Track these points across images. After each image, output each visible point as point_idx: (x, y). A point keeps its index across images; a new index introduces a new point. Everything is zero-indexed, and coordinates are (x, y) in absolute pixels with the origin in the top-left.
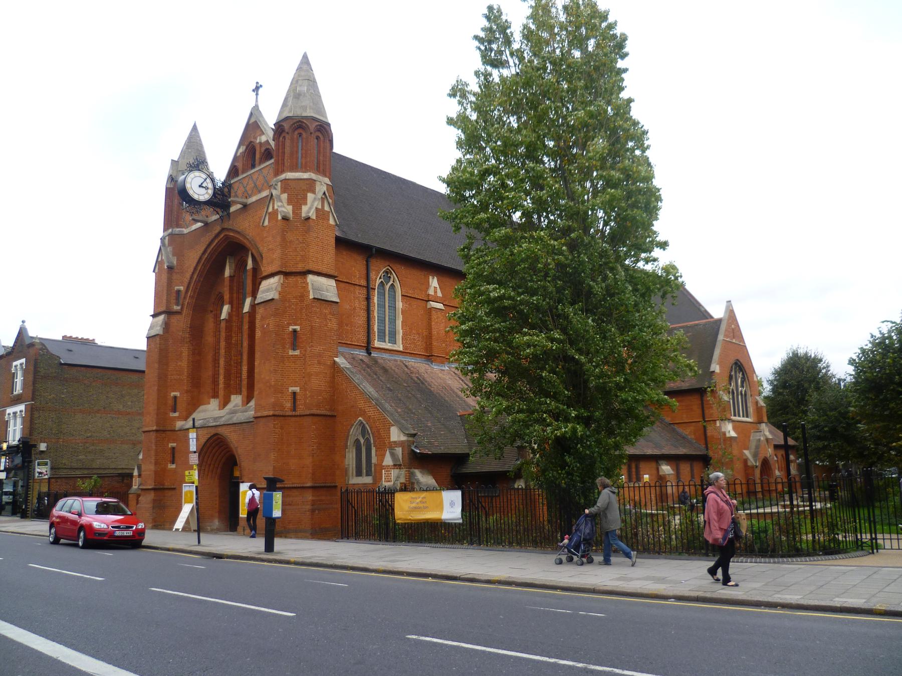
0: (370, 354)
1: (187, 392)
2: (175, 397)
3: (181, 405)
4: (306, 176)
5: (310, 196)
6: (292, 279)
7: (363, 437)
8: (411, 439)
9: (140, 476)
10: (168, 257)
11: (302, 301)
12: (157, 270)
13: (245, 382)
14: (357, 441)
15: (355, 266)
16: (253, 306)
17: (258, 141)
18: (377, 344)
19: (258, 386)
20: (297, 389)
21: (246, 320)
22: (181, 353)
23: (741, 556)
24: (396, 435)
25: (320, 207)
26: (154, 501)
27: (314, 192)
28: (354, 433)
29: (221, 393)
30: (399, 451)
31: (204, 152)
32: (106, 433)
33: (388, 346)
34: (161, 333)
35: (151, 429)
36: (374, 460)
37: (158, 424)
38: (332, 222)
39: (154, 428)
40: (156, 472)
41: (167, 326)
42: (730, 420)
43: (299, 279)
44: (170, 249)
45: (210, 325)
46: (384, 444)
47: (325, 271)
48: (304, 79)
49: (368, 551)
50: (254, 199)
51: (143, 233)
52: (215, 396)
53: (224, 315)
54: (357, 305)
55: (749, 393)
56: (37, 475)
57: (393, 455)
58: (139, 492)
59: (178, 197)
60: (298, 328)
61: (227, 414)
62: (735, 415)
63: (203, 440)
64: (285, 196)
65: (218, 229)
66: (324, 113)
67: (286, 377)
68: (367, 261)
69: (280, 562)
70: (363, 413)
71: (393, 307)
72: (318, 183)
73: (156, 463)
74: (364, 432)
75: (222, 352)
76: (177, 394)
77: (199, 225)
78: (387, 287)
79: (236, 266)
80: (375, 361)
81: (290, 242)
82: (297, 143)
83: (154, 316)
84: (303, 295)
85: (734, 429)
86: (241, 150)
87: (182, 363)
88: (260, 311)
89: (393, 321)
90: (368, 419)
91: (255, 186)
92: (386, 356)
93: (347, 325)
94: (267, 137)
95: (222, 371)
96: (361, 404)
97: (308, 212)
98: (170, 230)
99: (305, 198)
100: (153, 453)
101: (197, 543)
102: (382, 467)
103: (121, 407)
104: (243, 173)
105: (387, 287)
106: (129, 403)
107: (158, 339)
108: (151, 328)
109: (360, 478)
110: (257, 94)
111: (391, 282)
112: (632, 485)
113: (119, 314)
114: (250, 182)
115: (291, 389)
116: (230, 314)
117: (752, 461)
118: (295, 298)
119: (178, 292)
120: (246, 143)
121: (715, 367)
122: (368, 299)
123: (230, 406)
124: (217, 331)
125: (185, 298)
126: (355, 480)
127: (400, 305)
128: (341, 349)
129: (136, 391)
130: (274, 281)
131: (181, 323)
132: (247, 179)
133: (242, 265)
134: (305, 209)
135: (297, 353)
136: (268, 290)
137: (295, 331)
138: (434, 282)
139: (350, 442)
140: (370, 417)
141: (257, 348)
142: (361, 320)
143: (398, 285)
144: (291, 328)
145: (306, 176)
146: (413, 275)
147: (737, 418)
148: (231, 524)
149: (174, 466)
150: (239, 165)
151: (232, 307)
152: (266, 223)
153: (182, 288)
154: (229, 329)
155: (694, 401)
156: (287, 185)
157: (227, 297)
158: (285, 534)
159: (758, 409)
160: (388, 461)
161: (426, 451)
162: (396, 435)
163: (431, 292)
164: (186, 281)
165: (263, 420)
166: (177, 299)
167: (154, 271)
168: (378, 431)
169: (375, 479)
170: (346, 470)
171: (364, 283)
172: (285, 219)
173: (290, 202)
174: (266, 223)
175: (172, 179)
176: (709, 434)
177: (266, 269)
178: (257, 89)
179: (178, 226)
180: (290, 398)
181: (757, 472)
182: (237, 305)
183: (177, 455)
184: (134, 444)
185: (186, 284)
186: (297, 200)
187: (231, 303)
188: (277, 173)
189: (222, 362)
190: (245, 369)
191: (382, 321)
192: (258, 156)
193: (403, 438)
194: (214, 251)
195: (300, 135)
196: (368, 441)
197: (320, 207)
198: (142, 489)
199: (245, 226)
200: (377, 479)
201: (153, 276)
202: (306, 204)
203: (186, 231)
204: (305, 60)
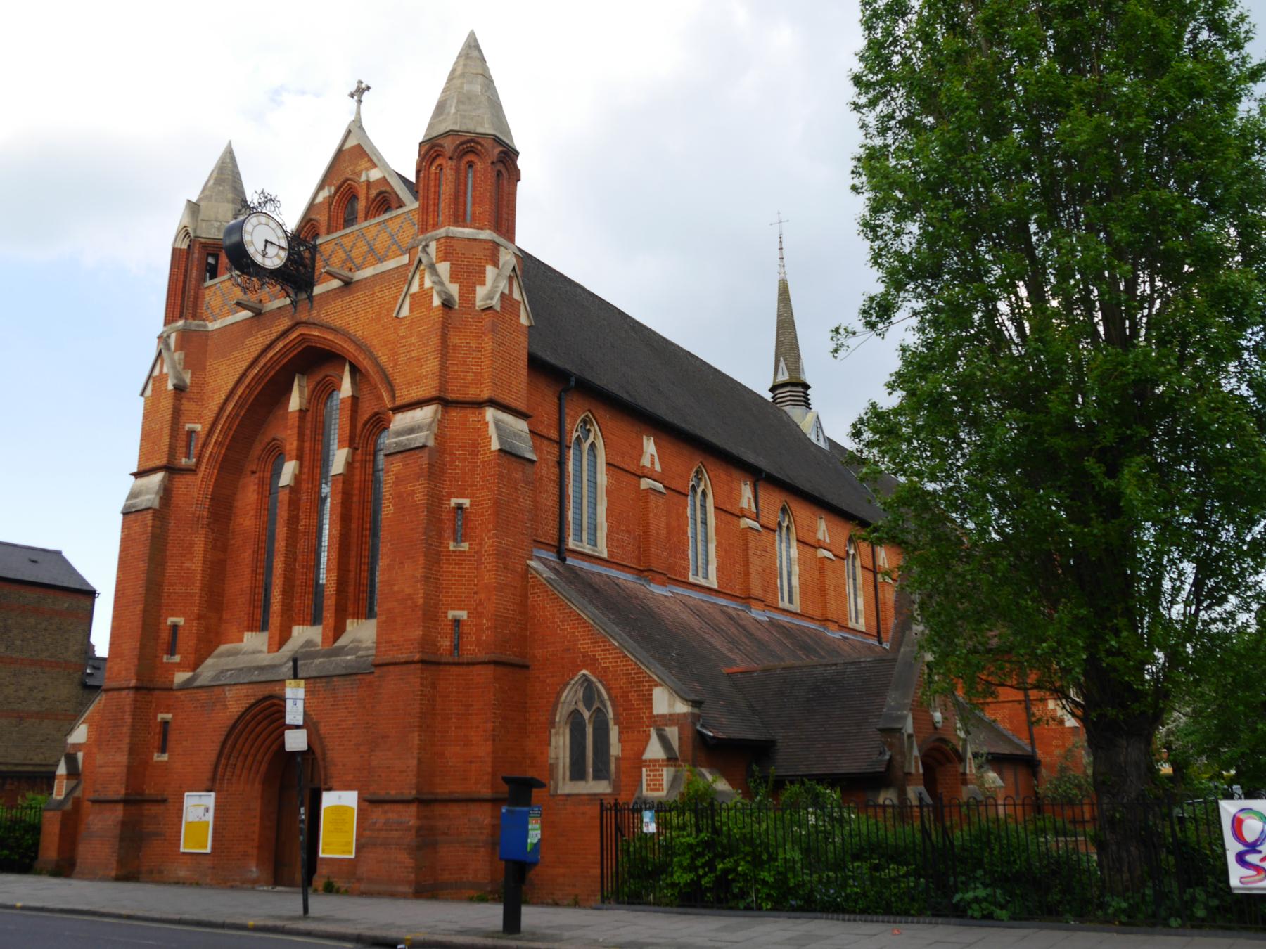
0: (563, 559)
1: (199, 617)
2: (175, 627)
3: (187, 641)
5: (490, 271)
6: (456, 414)
11: (474, 454)
12: (148, 392)
17: (363, 178)
18: (571, 544)
20: (463, 615)
22: (192, 544)
23: (876, 913)
25: (507, 292)
26: (123, 824)
28: (570, 697)
29: (275, 621)
30: (673, 732)
34: (156, 505)
35: (124, 684)
36: (615, 749)
37: (139, 675)
38: (524, 320)
39: (417, 657)
40: (130, 768)
41: (166, 493)
43: (470, 415)
44: (178, 356)
45: (249, 495)
49: (582, 927)
50: (368, 272)
54: (544, 472)
60: (466, 502)
65: (286, 323)
68: (560, 399)
70: (591, 662)
73: (132, 751)
74: (590, 695)
75: (280, 544)
76: (180, 621)
80: (571, 569)
81: (455, 347)
82: (466, 174)
83: (137, 475)
86: (325, 193)
87: (192, 561)
90: (603, 674)
91: (372, 250)
98: (180, 323)
99: (483, 272)
100: (126, 730)
101: (301, 912)
104: (328, 233)
105: (586, 445)
106: (18, 642)
107: (149, 515)
109: (582, 783)
110: (360, 101)
114: (360, 244)
116: (297, 478)
118: (463, 447)
120: (337, 182)
122: (561, 464)
125: (205, 445)
126: (567, 787)
129: (32, 621)
130: (424, 414)
131: (195, 490)
132: (399, 220)
134: (481, 292)
135: (465, 546)
138: (649, 446)
139: (561, 715)
146: (622, 428)
149: (165, 757)
150: (322, 219)
151: (301, 466)
152: (405, 312)
153: (198, 427)
154: (294, 504)
156: (449, 250)
157: (291, 445)
161: (721, 735)
162: (664, 702)
163: (646, 462)
164: (209, 415)
165: (397, 669)
167: (142, 394)
168: (625, 696)
169: (616, 786)
171: (554, 435)
174: (405, 312)
178: (360, 91)
179: (194, 316)
184: (21, 718)
185: (209, 421)
187: (300, 458)
189: (279, 564)
192: (361, 205)
193: (682, 708)
195: (471, 165)
197: (507, 292)
201: (139, 405)
202: (483, 283)
203: (212, 326)
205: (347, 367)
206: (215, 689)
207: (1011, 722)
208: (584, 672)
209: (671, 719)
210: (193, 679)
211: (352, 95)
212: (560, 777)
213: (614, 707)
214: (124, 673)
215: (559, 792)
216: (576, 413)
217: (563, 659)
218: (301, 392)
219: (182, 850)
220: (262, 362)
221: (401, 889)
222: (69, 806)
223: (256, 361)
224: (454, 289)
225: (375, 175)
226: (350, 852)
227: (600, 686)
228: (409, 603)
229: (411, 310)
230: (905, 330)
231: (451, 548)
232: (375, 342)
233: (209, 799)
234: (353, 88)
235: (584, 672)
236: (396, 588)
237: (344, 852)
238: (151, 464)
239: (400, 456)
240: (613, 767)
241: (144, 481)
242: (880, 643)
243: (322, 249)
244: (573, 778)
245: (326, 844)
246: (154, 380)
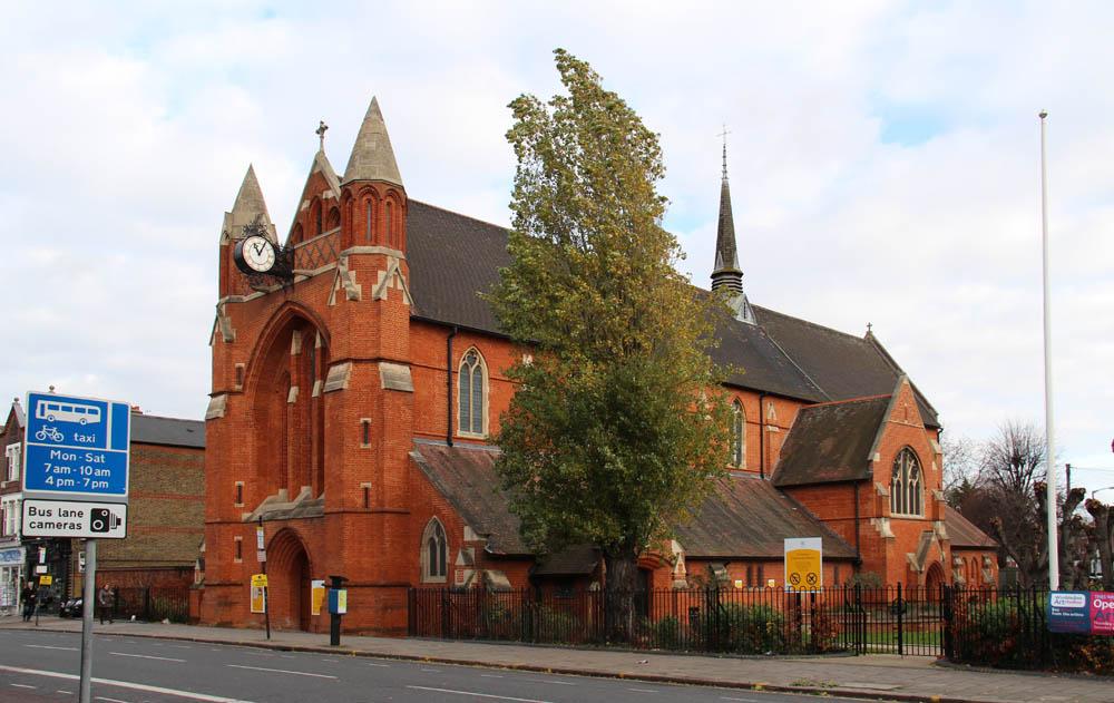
0: (451, 445)
2: (240, 487)
4: (376, 250)
5: (381, 274)
6: (362, 367)
7: (438, 536)
8: (484, 539)
9: (202, 569)
10: (226, 329)
12: (214, 343)
13: (315, 474)
14: (432, 539)
15: (434, 346)
16: (323, 393)
19: (327, 481)
20: (369, 485)
21: (315, 405)
24: (469, 535)
27: (384, 268)
28: (429, 532)
29: (290, 484)
30: (472, 551)
31: (263, 202)
32: (158, 520)
33: (472, 435)
36: (448, 560)
41: (228, 408)
42: (887, 517)
44: (228, 319)
46: (457, 544)
47: (398, 356)
51: (198, 294)
52: (284, 486)
53: (292, 398)
54: (437, 391)
55: (922, 485)
56: (81, 568)
57: (466, 555)
58: (202, 587)
59: (233, 265)
60: (369, 420)
61: (298, 506)
62: (899, 512)
63: (271, 535)
64: (353, 274)
65: (281, 301)
66: (396, 174)
67: (358, 475)
69: (345, 653)
70: (437, 511)
71: (479, 392)
72: (389, 258)
74: (438, 529)
76: (242, 483)
77: (259, 294)
78: (472, 370)
79: (303, 343)
80: (456, 453)
84: (375, 384)
85: (892, 527)
88: (329, 401)
89: (479, 408)
92: (469, 447)
93: (425, 414)
94: (334, 193)
95: (290, 460)
96: (436, 502)
97: (378, 292)
98: (227, 298)
102: (456, 567)
103: (175, 490)
105: (472, 370)
108: (210, 409)
110: (322, 137)
111: (477, 364)
112: (751, 589)
113: (177, 380)
115: (363, 485)
117: (915, 566)
119: (240, 369)
121: (876, 457)
122: (449, 384)
123: (300, 498)
124: (285, 414)
126: (428, 579)
127: (486, 389)
128: (418, 441)
131: (243, 404)
133: (308, 342)
134: (375, 288)
135: (369, 446)
136: (336, 378)
137: (366, 423)
139: (425, 540)
141: (326, 440)
142: (440, 407)
143: (484, 366)
144: (362, 420)
145: (376, 250)
147: (895, 515)
148: (305, 623)
152: (334, 303)
153: (243, 365)
154: (297, 413)
155: (847, 494)
157: (294, 377)
158: (348, 632)
159: (935, 505)
160: (460, 561)
161: (501, 552)
162: (469, 535)
165: (333, 516)
166: (239, 376)
167: (211, 344)
170: (421, 569)
171: (445, 367)
172: (354, 299)
173: (358, 280)
174: (334, 303)
175: (225, 252)
176: (861, 532)
177: (336, 355)
178: (322, 130)
180: (362, 493)
181: (922, 580)
182: (306, 388)
183: (243, 548)
186: (367, 278)
187: (298, 385)
188: (343, 248)
190: (315, 459)
191: (465, 408)
194: (275, 313)
196: (443, 539)
198: (206, 585)
199: (309, 299)
200: (450, 578)
204: (374, 108)
207: (846, 534)
209: (472, 544)
210: (251, 517)
211: (318, 132)
216: (462, 350)
218: (297, 343)
223: (268, 324)
230: (695, 264)
238: (221, 389)
241: (215, 399)
242: (762, 477)
244: (432, 575)
246: (216, 335)
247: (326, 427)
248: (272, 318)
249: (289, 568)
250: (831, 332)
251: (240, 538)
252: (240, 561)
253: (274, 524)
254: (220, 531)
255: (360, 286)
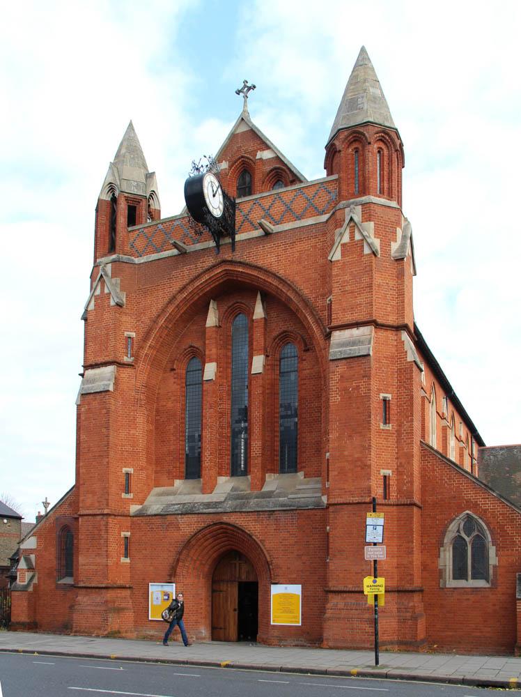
2: (128, 474)
48: (362, 76)
60: (389, 396)
65: (210, 261)
76: (131, 470)
81: (379, 286)
91: (289, 210)
126: (451, 583)
135: (389, 427)
139: (448, 539)
140: (485, 511)
144: (382, 395)
165: (350, 507)
168: (502, 527)
173: (377, 234)
180: (381, 482)
192: (258, 176)
202: (395, 241)
205: (259, 297)
206: (169, 517)
208: (467, 512)
212: (447, 577)
213: (492, 534)
214: (97, 504)
215: (447, 586)
217: (450, 503)
219: (150, 619)
220: (190, 289)
221: (367, 645)
222: (31, 589)
224: (377, 243)
225: (266, 155)
226: (298, 622)
227: (480, 521)
228: (359, 463)
229: (343, 255)
231: (381, 428)
232: (297, 278)
233: (296, 589)
234: (241, 86)
235: (467, 512)
236: (346, 453)
237: (291, 622)
239: (344, 361)
240: (491, 572)
243: (241, 207)
245: (275, 617)
247: (332, 400)
248: (192, 281)
249: (206, 568)
250: (438, 365)
251: (128, 534)
252: (128, 560)
253: (194, 518)
254: (106, 525)
255: (379, 240)
